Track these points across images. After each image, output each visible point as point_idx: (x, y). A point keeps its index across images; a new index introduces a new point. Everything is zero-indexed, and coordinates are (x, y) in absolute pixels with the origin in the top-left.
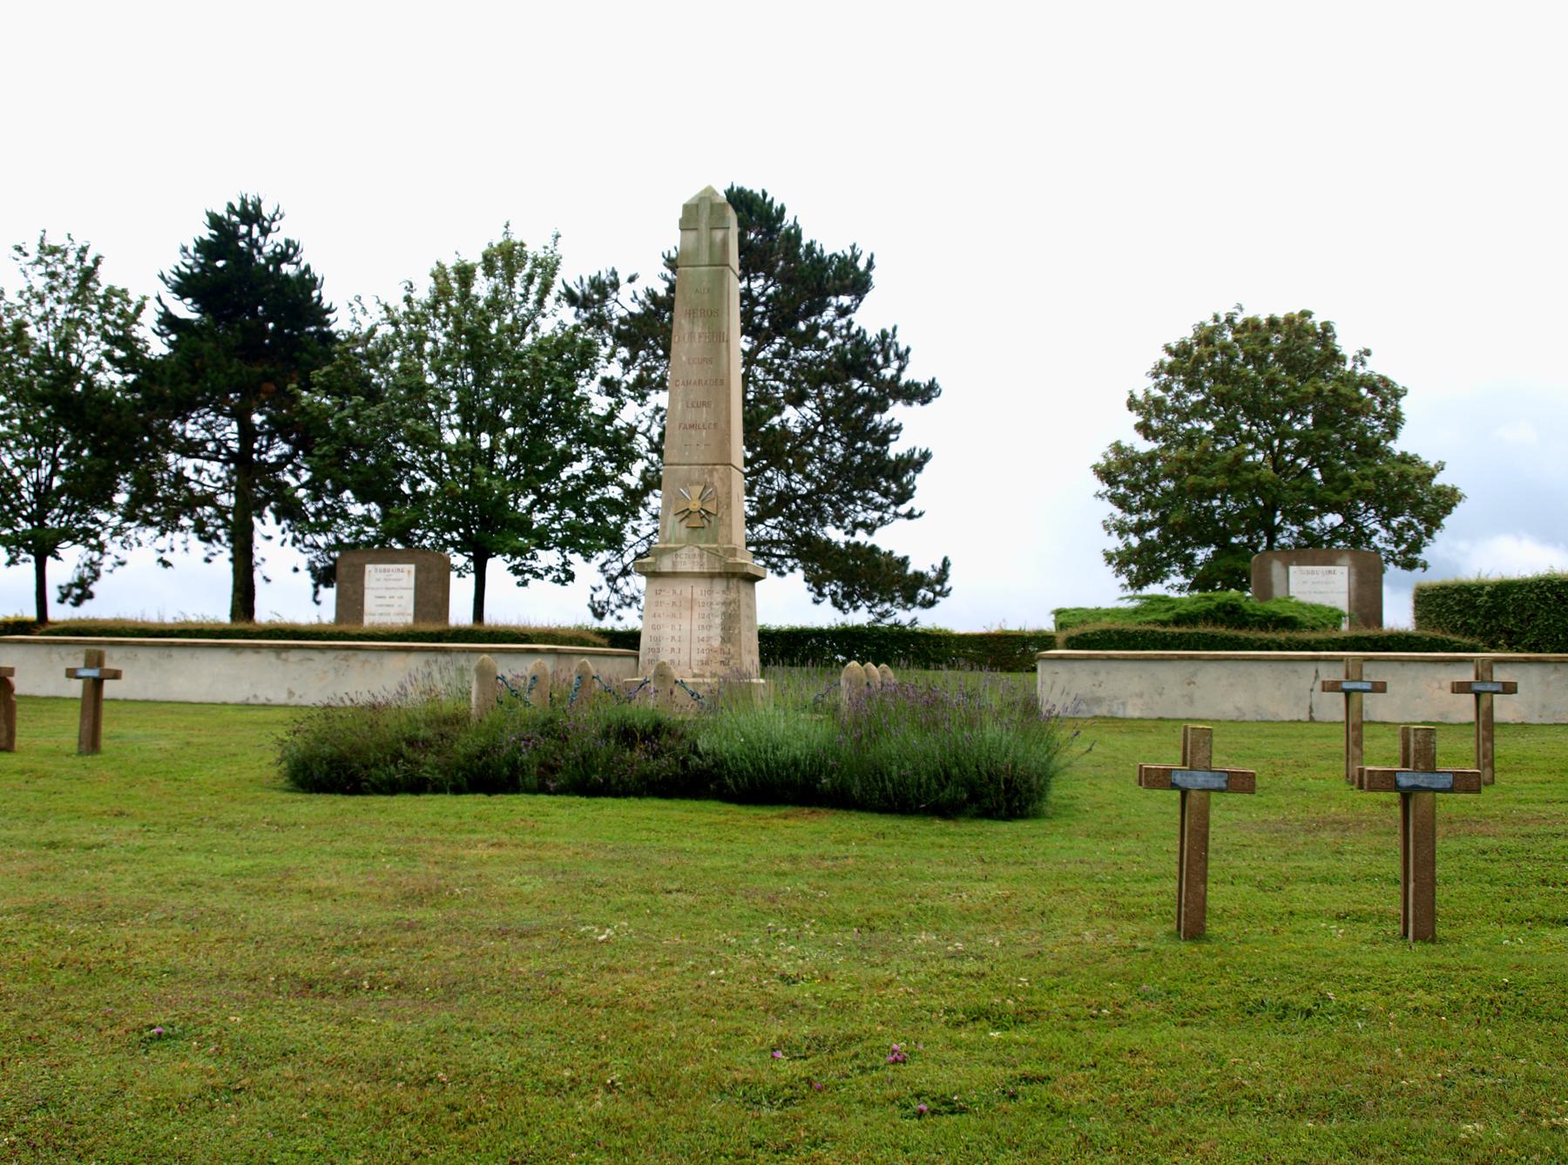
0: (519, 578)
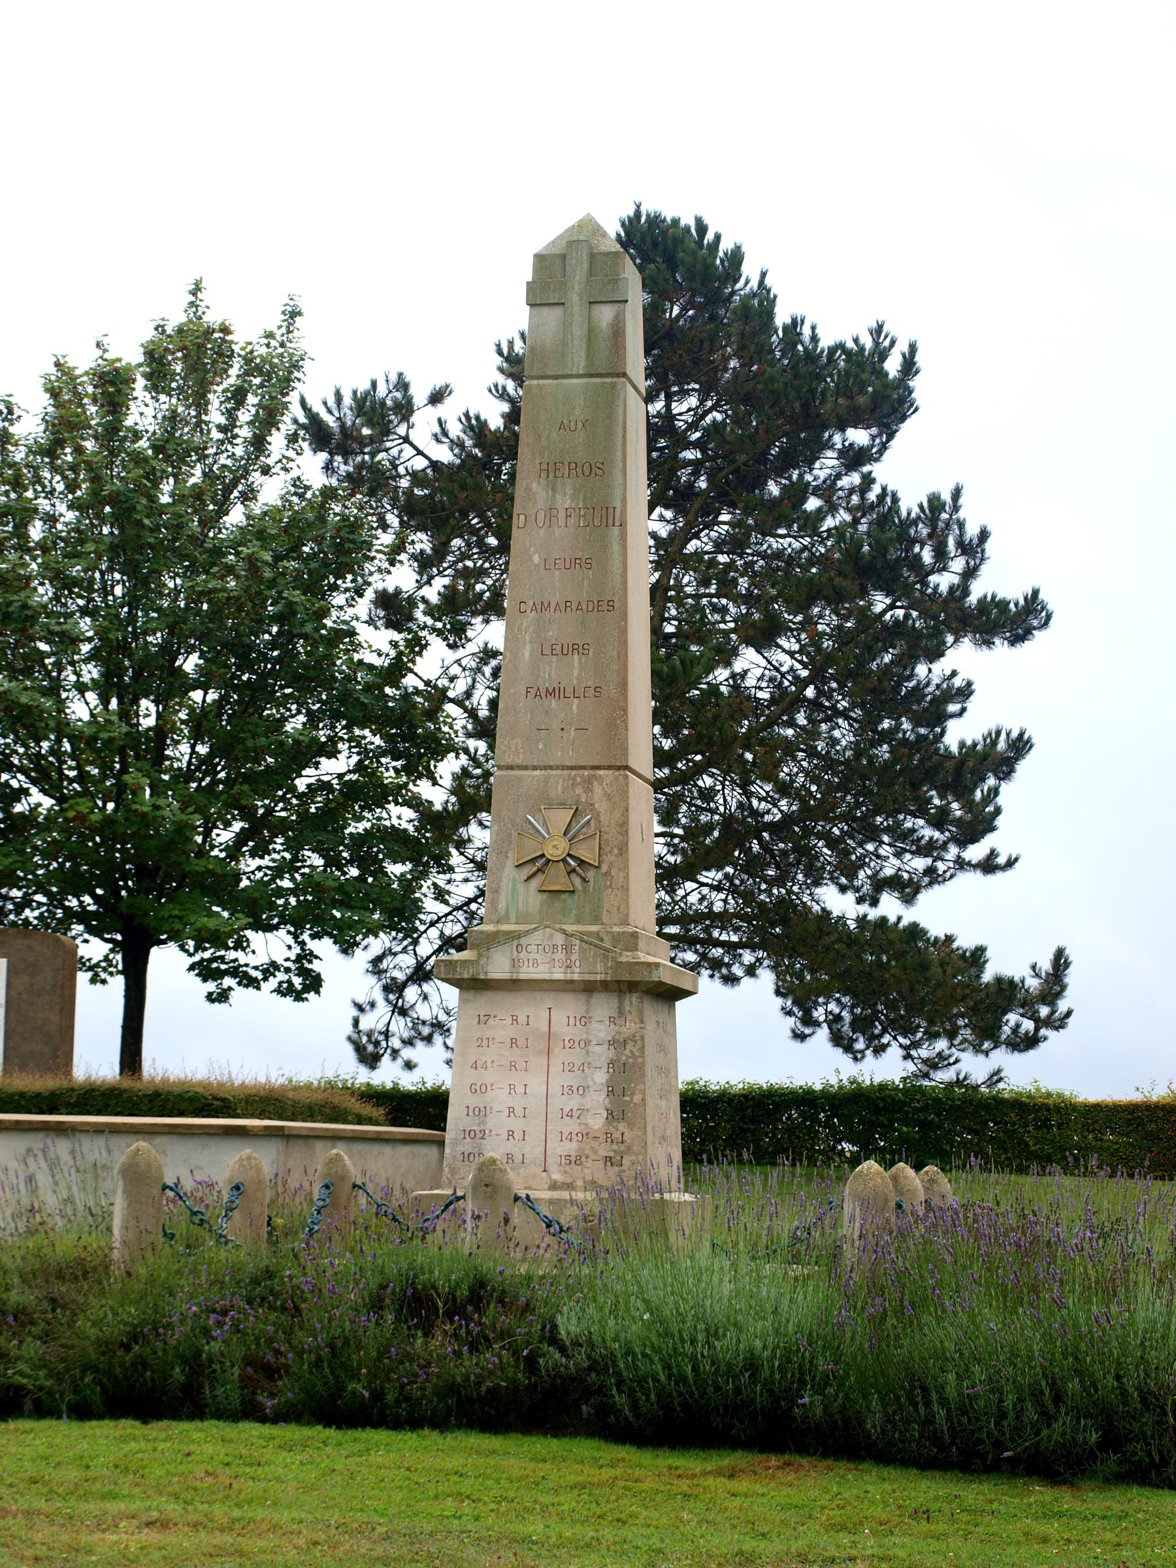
0: (211, 986)
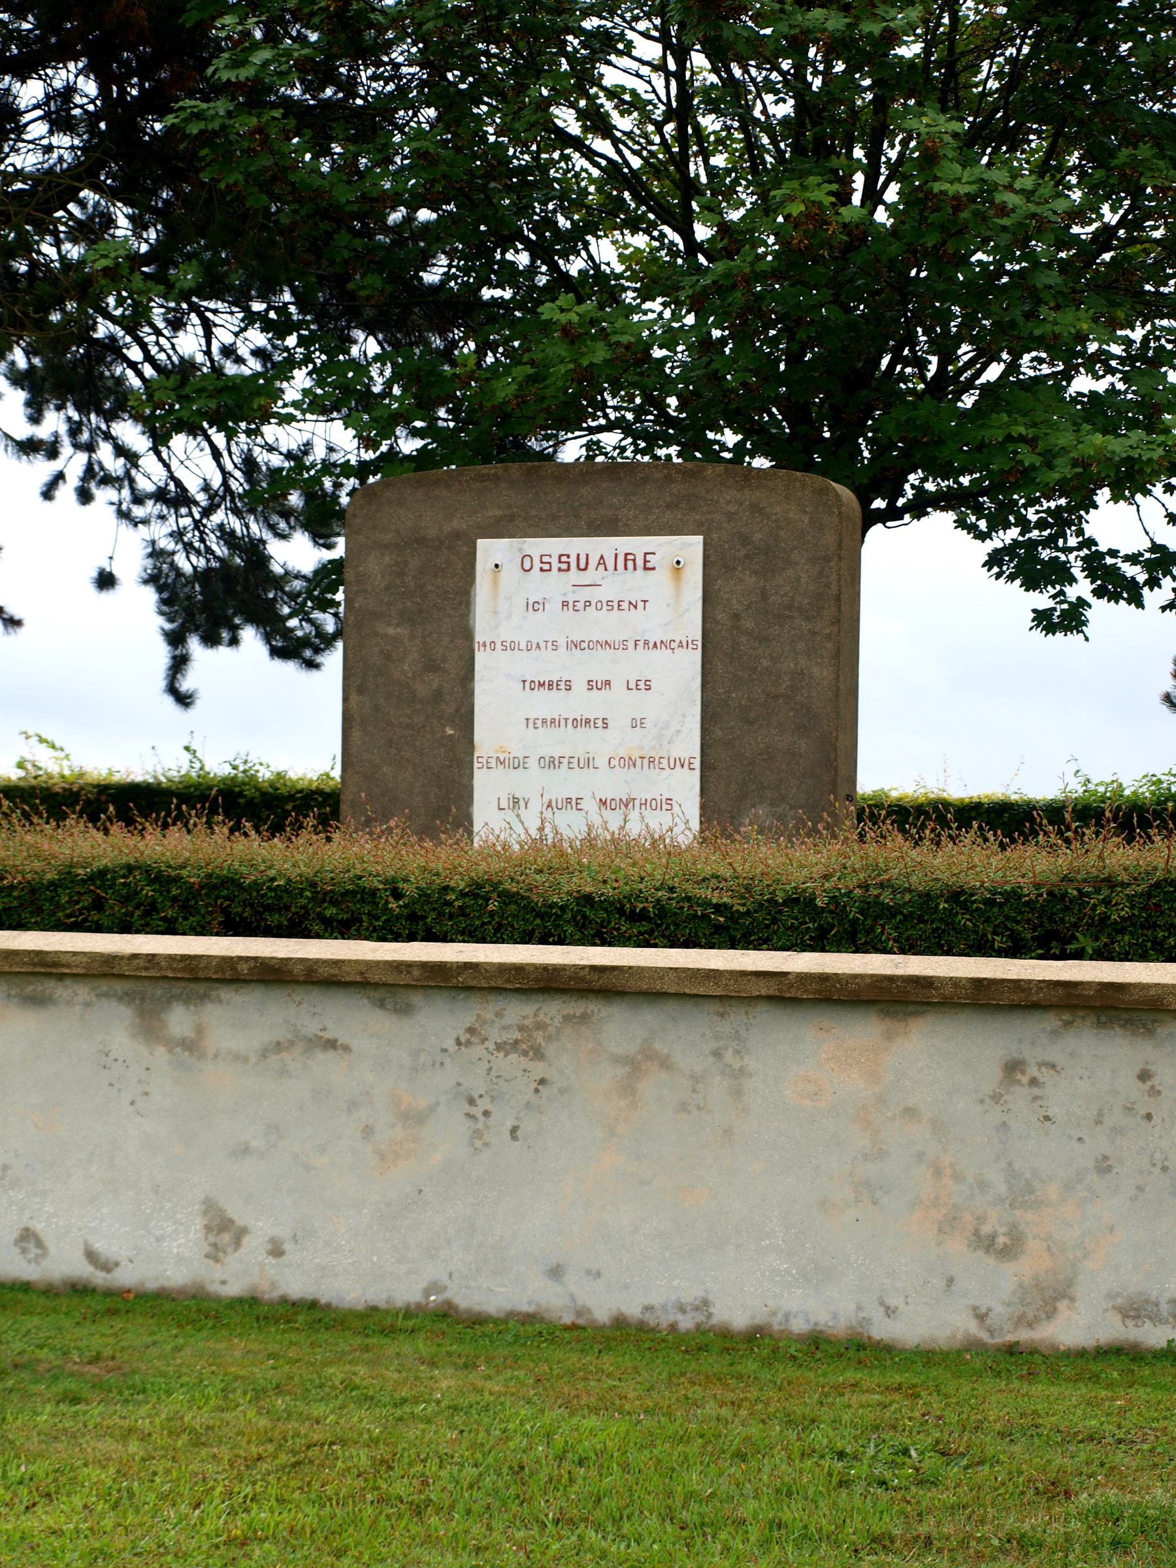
0: (1042, 600)
